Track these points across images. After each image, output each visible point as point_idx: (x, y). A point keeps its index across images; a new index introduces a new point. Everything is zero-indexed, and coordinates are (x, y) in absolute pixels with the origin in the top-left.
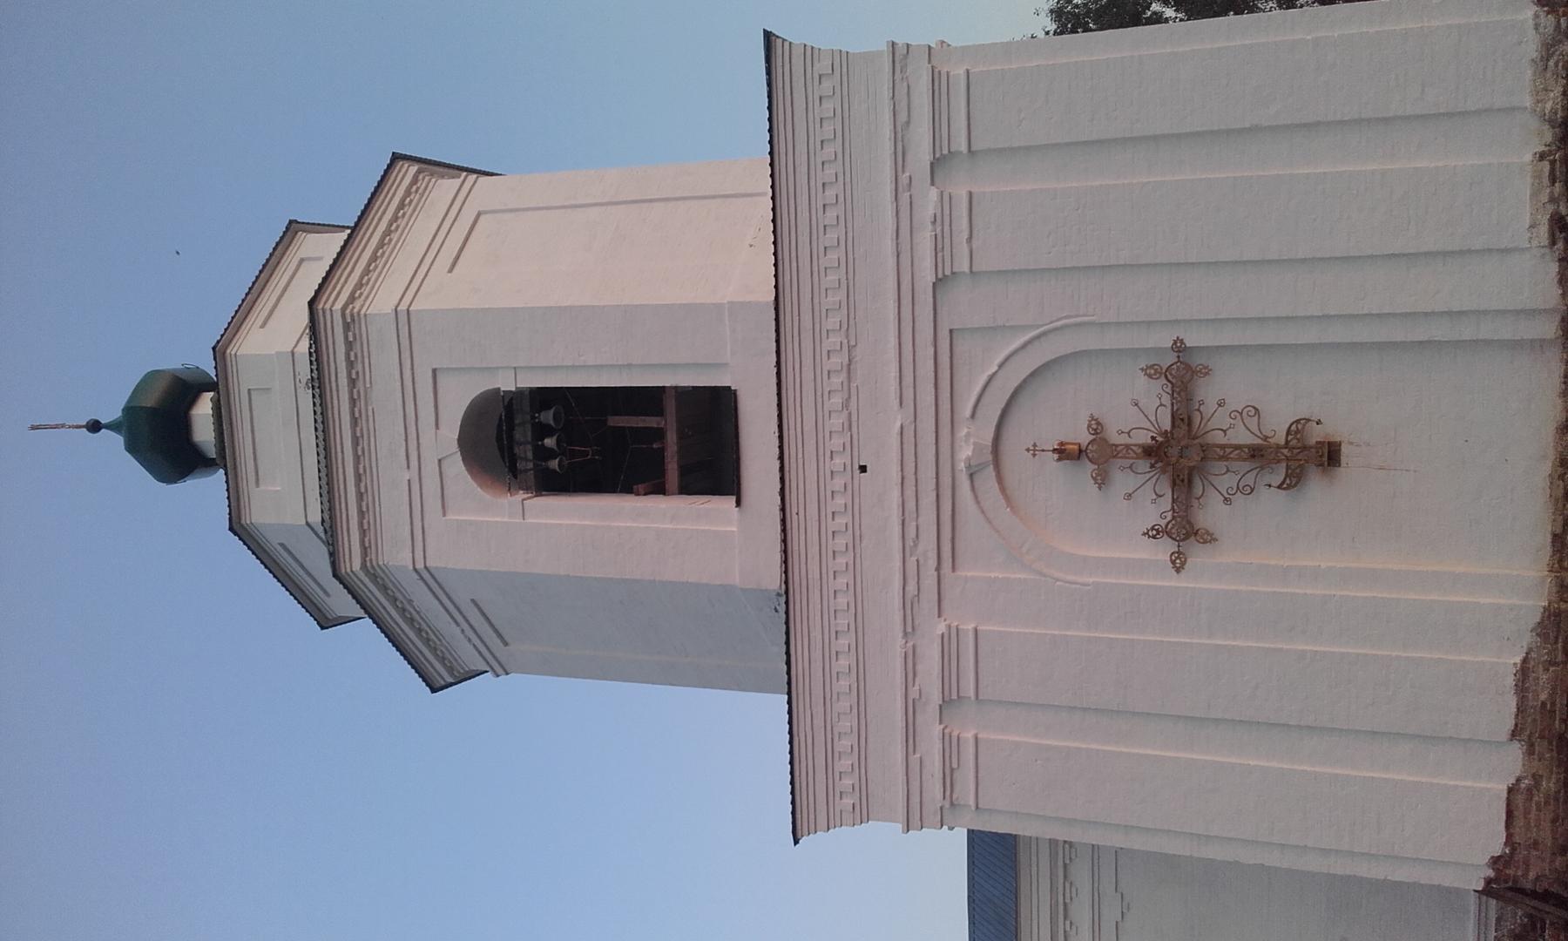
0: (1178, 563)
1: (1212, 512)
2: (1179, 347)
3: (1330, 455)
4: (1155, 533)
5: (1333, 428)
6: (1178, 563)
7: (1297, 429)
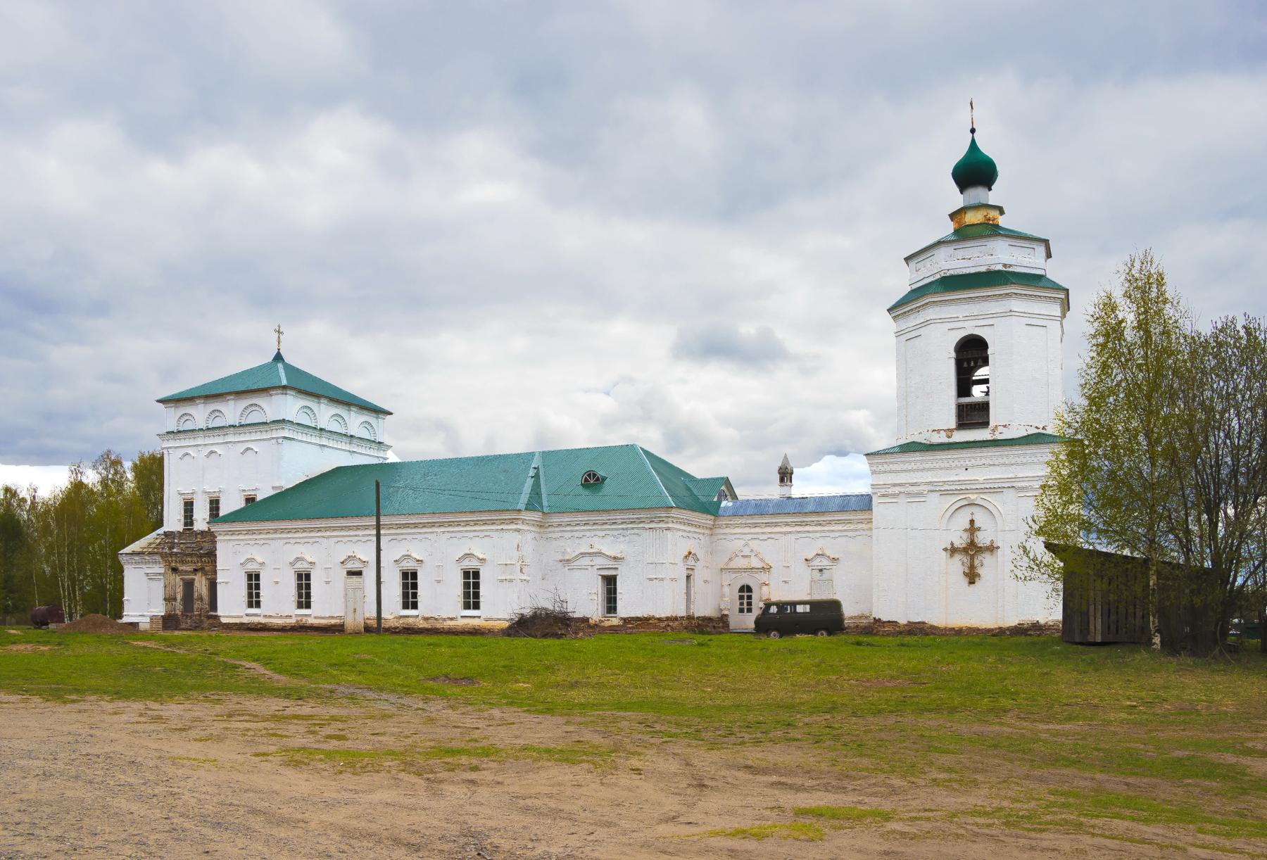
0: (945, 550)
1: (958, 557)
2: (998, 548)
3: (972, 582)
4: (952, 544)
5: (978, 583)
6: (945, 550)
7: (979, 575)
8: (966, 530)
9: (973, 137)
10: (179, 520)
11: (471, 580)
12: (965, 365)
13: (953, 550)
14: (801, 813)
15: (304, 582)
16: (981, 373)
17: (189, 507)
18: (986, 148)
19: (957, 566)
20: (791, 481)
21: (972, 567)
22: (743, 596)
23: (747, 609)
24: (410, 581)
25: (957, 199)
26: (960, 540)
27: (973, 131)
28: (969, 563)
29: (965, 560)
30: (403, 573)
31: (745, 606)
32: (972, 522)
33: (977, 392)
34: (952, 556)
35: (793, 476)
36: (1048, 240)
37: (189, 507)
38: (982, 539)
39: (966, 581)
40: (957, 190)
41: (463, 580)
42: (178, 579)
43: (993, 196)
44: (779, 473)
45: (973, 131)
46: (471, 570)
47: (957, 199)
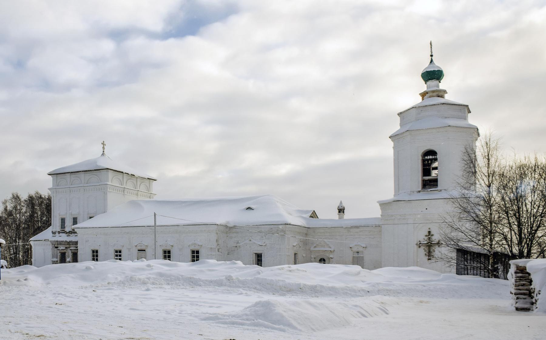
9: (432, 58)
11: (167, 255)
15: (167, 255)
16: (435, 165)
17: (63, 221)
20: (344, 213)
23: (119, 256)
24: (195, 255)
25: (423, 87)
27: (432, 56)
28: (428, 250)
29: (426, 249)
30: (164, 251)
32: (429, 232)
33: (434, 173)
35: (345, 210)
36: (468, 106)
37: (63, 221)
40: (424, 82)
42: (58, 252)
43: (443, 85)
44: (338, 209)
45: (432, 56)
46: (167, 250)
47: (423, 87)
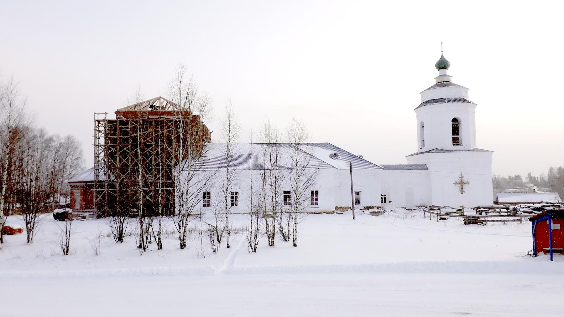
6: (454, 183)
8: (460, 177)
10: (275, 243)
12: (454, 126)
13: (456, 183)
14: (90, 214)
15: (287, 195)
18: (447, 58)
19: (458, 187)
21: (462, 189)
22: (235, 194)
25: (437, 73)
26: (458, 180)
27: (442, 51)
31: (383, 201)
34: (456, 185)
38: (465, 180)
39: (460, 193)
41: (314, 190)
45: (442, 51)
